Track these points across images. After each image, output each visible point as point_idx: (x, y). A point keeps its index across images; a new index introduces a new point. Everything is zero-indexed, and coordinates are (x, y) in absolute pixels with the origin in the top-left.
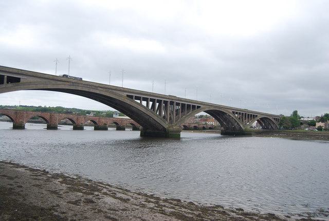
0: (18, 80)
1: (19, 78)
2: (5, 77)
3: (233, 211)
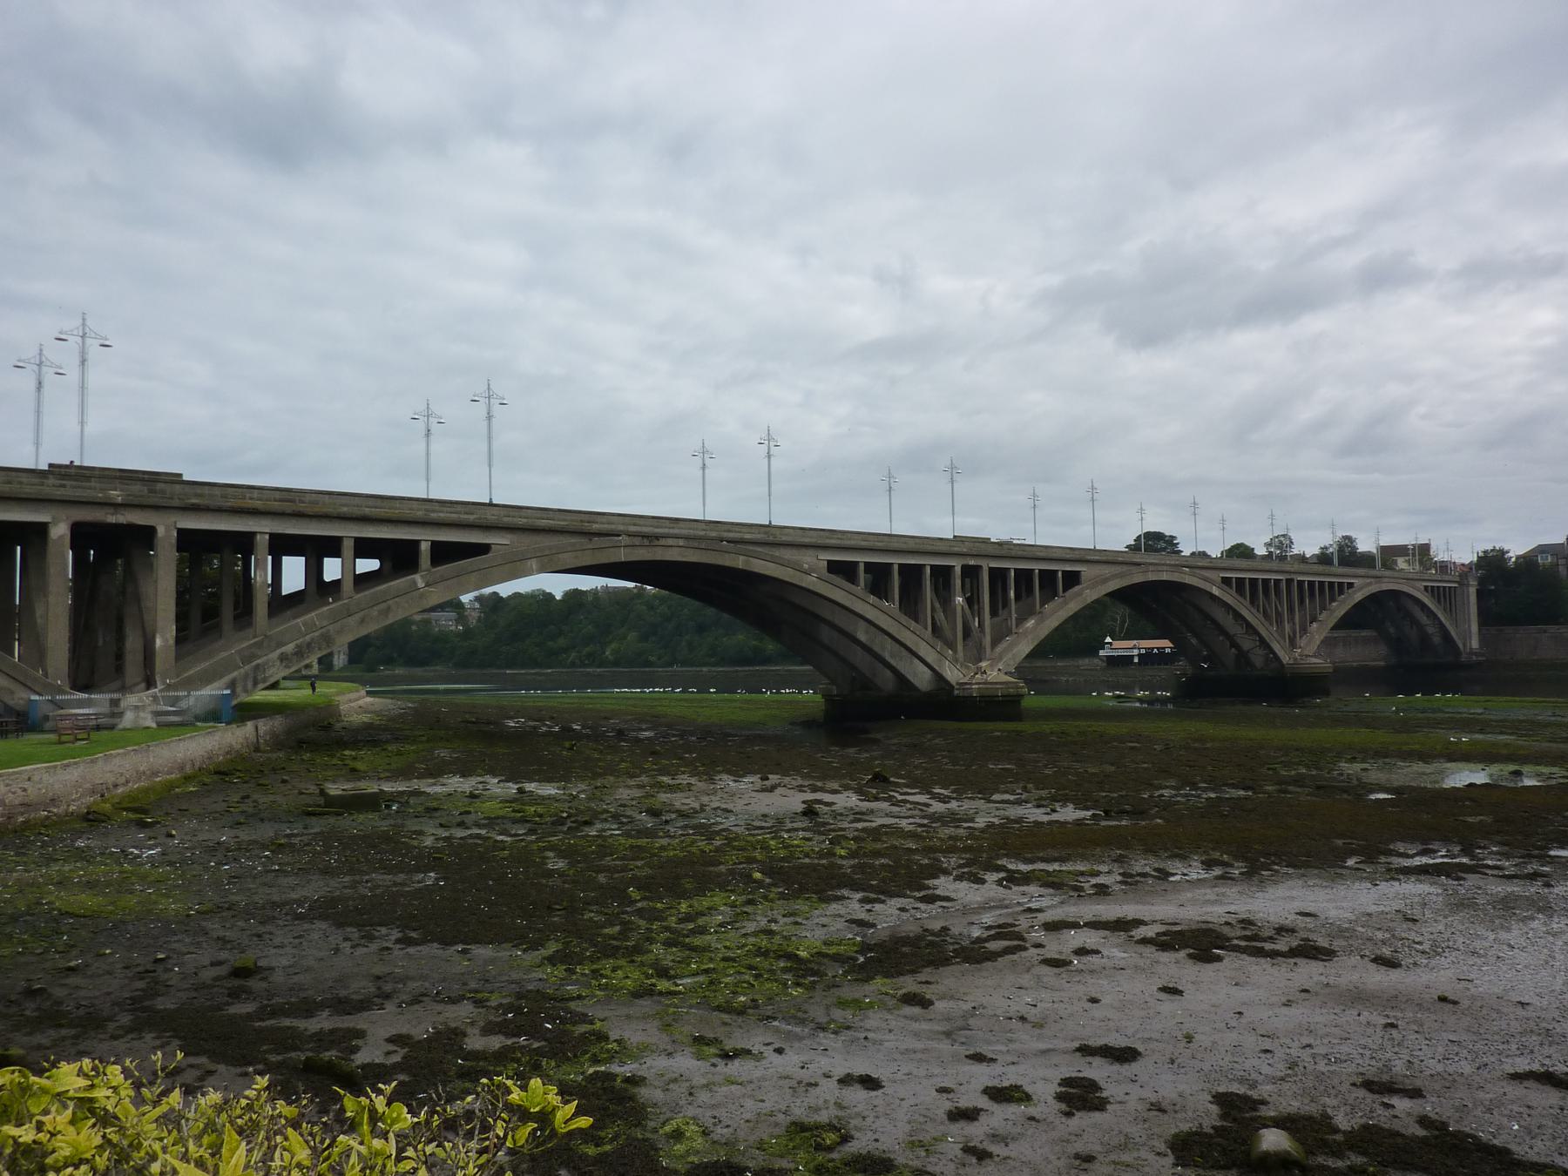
0: (483, 549)
1: (1353, 583)
2: (425, 547)
3: (1087, 819)
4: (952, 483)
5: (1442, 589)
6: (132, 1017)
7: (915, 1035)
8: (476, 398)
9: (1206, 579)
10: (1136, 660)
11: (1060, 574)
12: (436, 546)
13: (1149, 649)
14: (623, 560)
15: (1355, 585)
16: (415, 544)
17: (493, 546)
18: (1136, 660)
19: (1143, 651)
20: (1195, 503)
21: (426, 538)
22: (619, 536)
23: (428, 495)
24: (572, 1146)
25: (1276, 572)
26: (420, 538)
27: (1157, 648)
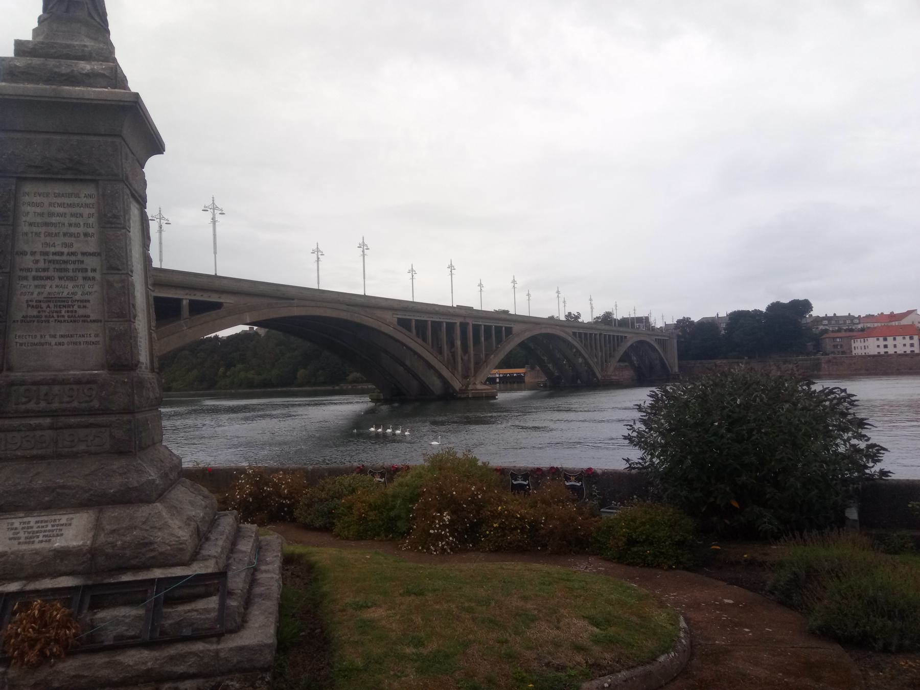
0: (218, 306)
4: (364, 257)
5: (620, 337)
6: (792, 577)
7: (492, 621)
8: (206, 209)
9: (566, 333)
10: (498, 380)
11: (504, 329)
12: (192, 303)
13: (505, 374)
14: (296, 315)
15: (628, 337)
16: (179, 301)
17: (224, 304)
18: (498, 380)
19: (501, 376)
20: (318, 250)
21: (185, 297)
22: (293, 300)
23: (161, 266)
24: (591, 663)
25: (661, 336)
26: (181, 297)
27: (509, 374)
